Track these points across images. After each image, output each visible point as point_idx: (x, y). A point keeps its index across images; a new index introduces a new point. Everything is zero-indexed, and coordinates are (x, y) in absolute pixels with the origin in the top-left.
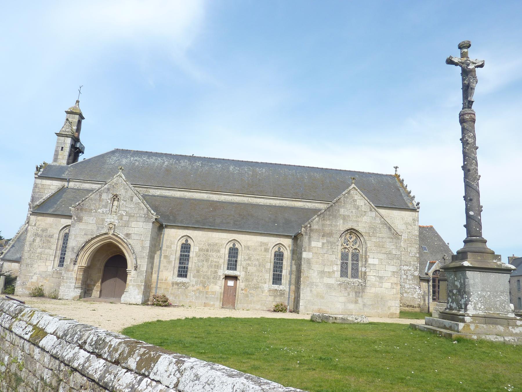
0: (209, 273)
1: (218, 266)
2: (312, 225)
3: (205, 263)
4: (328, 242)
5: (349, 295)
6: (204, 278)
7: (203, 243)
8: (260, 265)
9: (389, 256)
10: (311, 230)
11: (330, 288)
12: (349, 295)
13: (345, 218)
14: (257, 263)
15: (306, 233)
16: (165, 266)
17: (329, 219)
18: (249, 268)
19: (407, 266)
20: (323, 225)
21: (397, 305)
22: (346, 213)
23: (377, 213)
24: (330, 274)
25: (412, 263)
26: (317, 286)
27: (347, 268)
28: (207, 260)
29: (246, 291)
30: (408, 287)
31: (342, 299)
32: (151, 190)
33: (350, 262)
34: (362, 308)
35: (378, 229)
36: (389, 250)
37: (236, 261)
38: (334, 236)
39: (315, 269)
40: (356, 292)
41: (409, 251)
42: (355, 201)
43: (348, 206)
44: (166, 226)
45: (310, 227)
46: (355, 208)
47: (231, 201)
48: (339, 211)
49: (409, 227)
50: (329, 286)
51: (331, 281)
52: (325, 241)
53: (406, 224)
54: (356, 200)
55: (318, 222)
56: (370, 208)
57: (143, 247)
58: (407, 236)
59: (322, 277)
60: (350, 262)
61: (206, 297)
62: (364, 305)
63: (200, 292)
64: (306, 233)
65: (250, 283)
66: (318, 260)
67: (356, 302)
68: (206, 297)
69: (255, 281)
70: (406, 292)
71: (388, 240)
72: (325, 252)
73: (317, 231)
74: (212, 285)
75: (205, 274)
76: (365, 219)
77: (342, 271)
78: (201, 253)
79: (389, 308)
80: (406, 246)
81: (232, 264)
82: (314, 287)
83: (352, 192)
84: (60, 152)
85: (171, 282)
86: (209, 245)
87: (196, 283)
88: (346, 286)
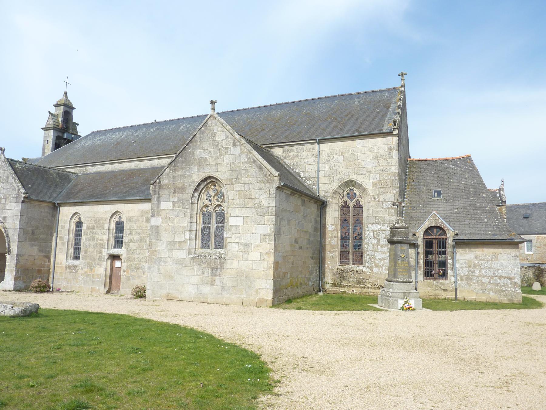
0: (95, 253)
1: (102, 245)
2: (161, 180)
3: (91, 242)
4: (180, 200)
5: (203, 272)
6: (91, 259)
7: (89, 219)
8: (141, 240)
9: (259, 210)
10: (161, 187)
11: (180, 264)
12: (203, 272)
13: (201, 163)
14: (138, 237)
15: (155, 191)
16: (60, 249)
17: (182, 168)
18: (131, 244)
19: (378, 223)
20: (174, 177)
21: (268, 287)
22: (203, 156)
23: (243, 148)
24: (180, 245)
25: (387, 218)
26: (165, 262)
27: (209, 235)
28: (93, 239)
29: (128, 272)
30: (381, 256)
31: (195, 279)
32: (89, 168)
33: (213, 225)
34: (220, 291)
35: (244, 172)
36: (259, 200)
37: (123, 237)
38: (187, 191)
39: (164, 239)
40: (212, 269)
41: (381, 200)
42: (214, 135)
43: (205, 145)
44: (60, 205)
45: (160, 182)
46: (214, 145)
47: (156, 166)
48: (193, 154)
49: (382, 162)
50: (179, 262)
51: (183, 254)
52: (176, 199)
53: (378, 158)
54: (215, 134)
55: (168, 175)
56: (234, 141)
57: (15, 229)
58: (378, 176)
59: (171, 250)
60: (213, 225)
61: (93, 282)
62: (223, 287)
63: (88, 276)
64: (155, 191)
65: (132, 263)
66: (167, 227)
67: (212, 284)
68: (93, 282)
69: (136, 260)
70: (377, 266)
71: (258, 186)
72: (176, 215)
73: (168, 186)
74: (97, 268)
75: (91, 254)
76: (228, 159)
77: (203, 239)
78: (89, 231)
79: (257, 292)
80: (376, 194)
81: (118, 243)
82: (163, 264)
83: (209, 122)
84: (46, 145)
85: (64, 266)
86: (95, 221)
87: (128, 267)
88: (199, 260)
